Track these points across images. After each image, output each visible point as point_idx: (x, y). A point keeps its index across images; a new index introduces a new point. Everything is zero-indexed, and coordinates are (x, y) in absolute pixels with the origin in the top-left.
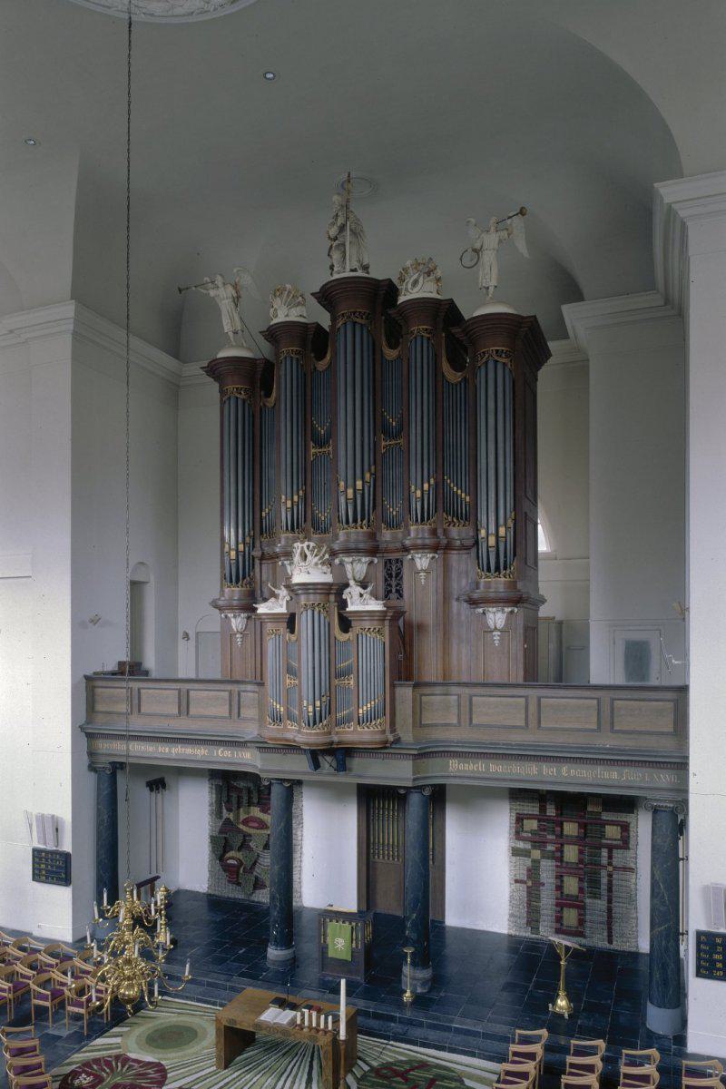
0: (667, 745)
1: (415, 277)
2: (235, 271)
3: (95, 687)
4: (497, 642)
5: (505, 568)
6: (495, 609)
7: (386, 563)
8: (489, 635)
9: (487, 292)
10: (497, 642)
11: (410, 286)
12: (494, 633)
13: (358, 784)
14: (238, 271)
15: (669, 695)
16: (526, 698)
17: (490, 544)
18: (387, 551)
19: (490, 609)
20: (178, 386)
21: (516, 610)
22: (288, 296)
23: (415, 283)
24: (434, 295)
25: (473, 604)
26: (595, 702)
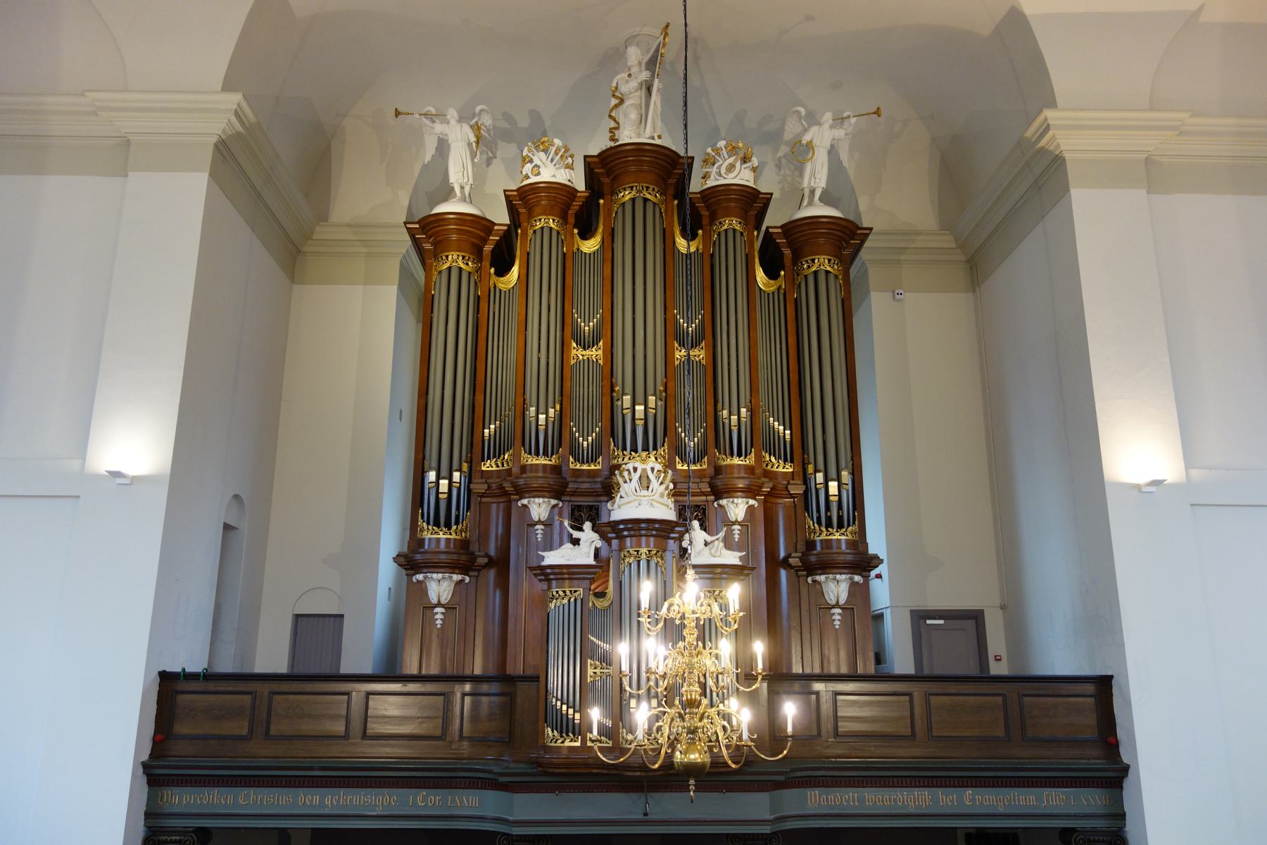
0: (1092, 759)
1: (731, 160)
2: (478, 109)
3: (836, 734)
4: (837, 623)
5: (457, 523)
6: (440, 576)
7: (573, 510)
8: (428, 612)
9: (806, 195)
10: (837, 623)
11: (723, 170)
12: (833, 611)
13: (313, 829)
14: (481, 111)
15: (1090, 688)
16: (910, 695)
17: (836, 484)
18: (574, 493)
19: (435, 576)
20: (299, 251)
21: (467, 579)
22: (556, 154)
23: (731, 168)
24: (751, 184)
25: (412, 569)
26: (1000, 699)
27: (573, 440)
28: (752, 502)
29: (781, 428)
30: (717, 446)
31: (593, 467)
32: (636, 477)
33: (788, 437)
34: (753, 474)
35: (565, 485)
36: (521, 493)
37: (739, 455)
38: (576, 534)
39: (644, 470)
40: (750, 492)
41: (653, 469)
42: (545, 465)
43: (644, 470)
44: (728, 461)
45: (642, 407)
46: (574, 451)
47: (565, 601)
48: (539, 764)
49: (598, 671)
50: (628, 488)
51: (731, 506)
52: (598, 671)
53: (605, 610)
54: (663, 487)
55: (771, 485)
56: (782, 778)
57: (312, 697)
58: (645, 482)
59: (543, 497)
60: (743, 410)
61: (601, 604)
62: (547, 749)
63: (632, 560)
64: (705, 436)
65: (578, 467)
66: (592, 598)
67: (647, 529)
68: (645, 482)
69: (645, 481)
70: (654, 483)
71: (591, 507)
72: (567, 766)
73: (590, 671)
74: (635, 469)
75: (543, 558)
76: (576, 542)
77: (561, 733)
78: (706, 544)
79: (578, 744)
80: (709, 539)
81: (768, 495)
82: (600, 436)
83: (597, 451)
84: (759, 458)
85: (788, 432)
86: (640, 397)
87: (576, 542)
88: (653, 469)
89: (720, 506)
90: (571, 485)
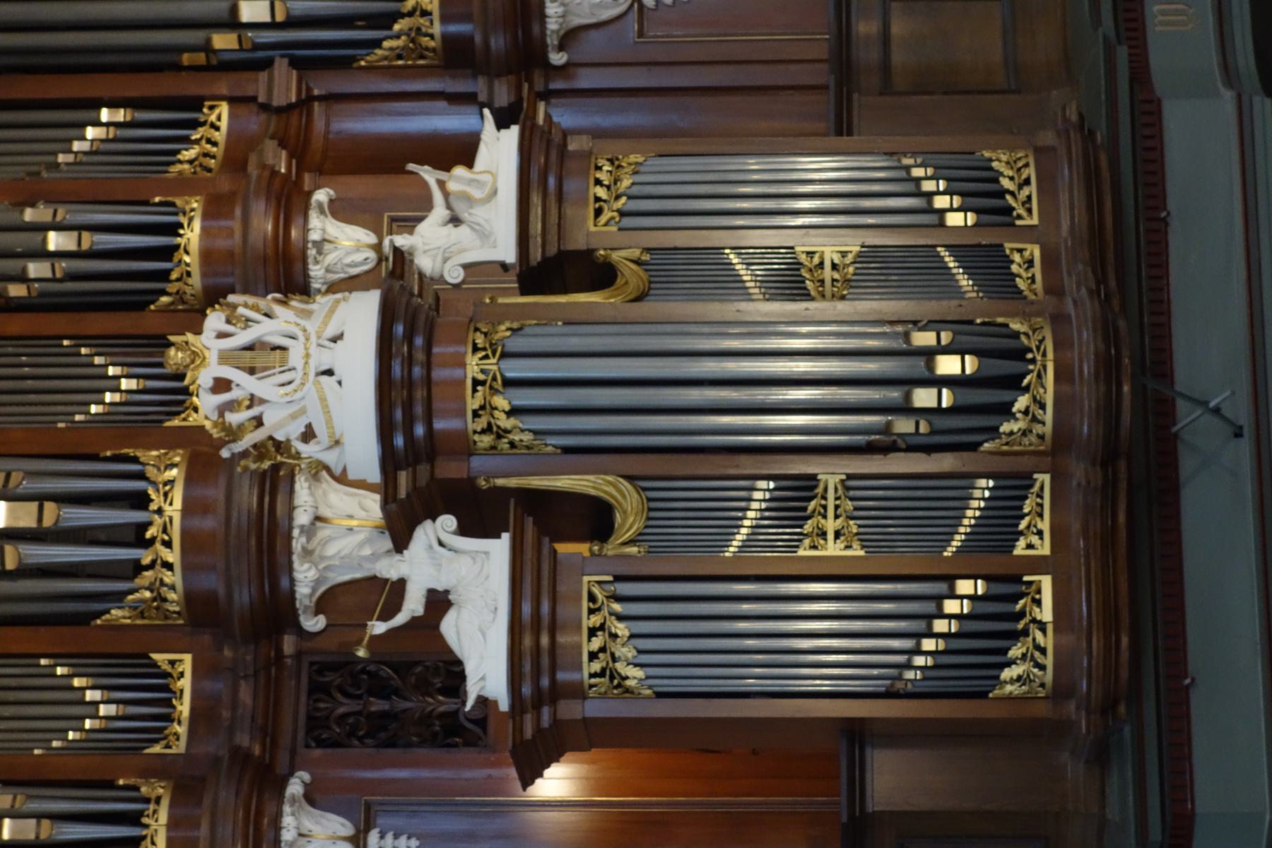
7: (321, 744)
27: (92, 743)
28: (295, 787)
29: (91, 132)
30: (138, 304)
31: (186, 684)
32: (245, 384)
33: (121, 115)
34: (232, 196)
35: (240, 758)
36: (277, 610)
37: (173, 229)
38: (413, 605)
39: (225, 358)
40: (289, 201)
41: (222, 335)
42: (172, 825)
43: (225, 358)
44: (191, 259)
45: (52, 235)
46: (124, 745)
47: (621, 629)
48: (1108, 707)
49: (831, 525)
50: (280, 409)
51: (330, 259)
52: (831, 525)
53: (652, 509)
54: (278, 309)
55: (270, 146)
56: (1122, 53)
57: (704, 232)
58: (258, 357)
59: (279, 815)
60: (29, 215)
61: (629, 521)
62: (1061, 691)
63: (501, 402)
64: (102, 342)
65: (182, 730)
66: (611, 548)
67: (409, 361)
68: (258, 357)
69: (259, 359)
70: (264, 330)
71: (317, 690)
72: (1110, 624)
73: (833, 549)
74: (222, 385)
75: (483, 701)
76: (439, 602)
77: (1015, 636)
78: (455, 220)
79: (1046, 582)
80: (439, 211)
81: (299, 151)
82: (79, 658)
83: (127, 663)
84: (185, 186)
85: (105, 115)
86: (30, 239)
87: (439, 602)
88: (222, 335)
89: (322, 605)
90: (243, 740)
